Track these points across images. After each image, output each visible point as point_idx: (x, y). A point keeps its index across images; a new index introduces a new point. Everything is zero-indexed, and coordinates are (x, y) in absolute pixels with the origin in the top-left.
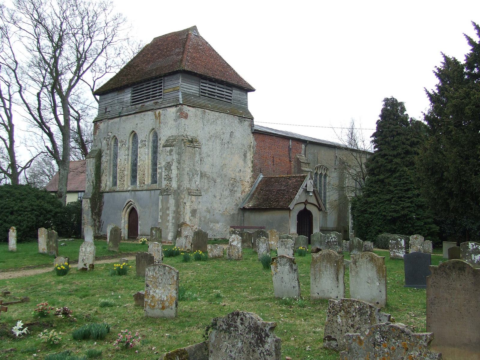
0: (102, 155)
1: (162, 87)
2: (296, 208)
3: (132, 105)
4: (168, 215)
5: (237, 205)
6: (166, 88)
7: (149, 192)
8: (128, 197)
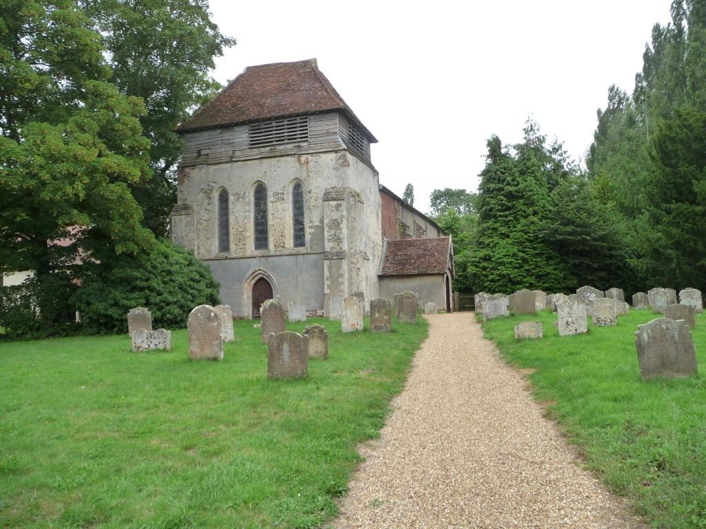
0: (683, 26)
3: (250, 148)
4: (342, 283)
6: (312, 129)
7: (294, 257)
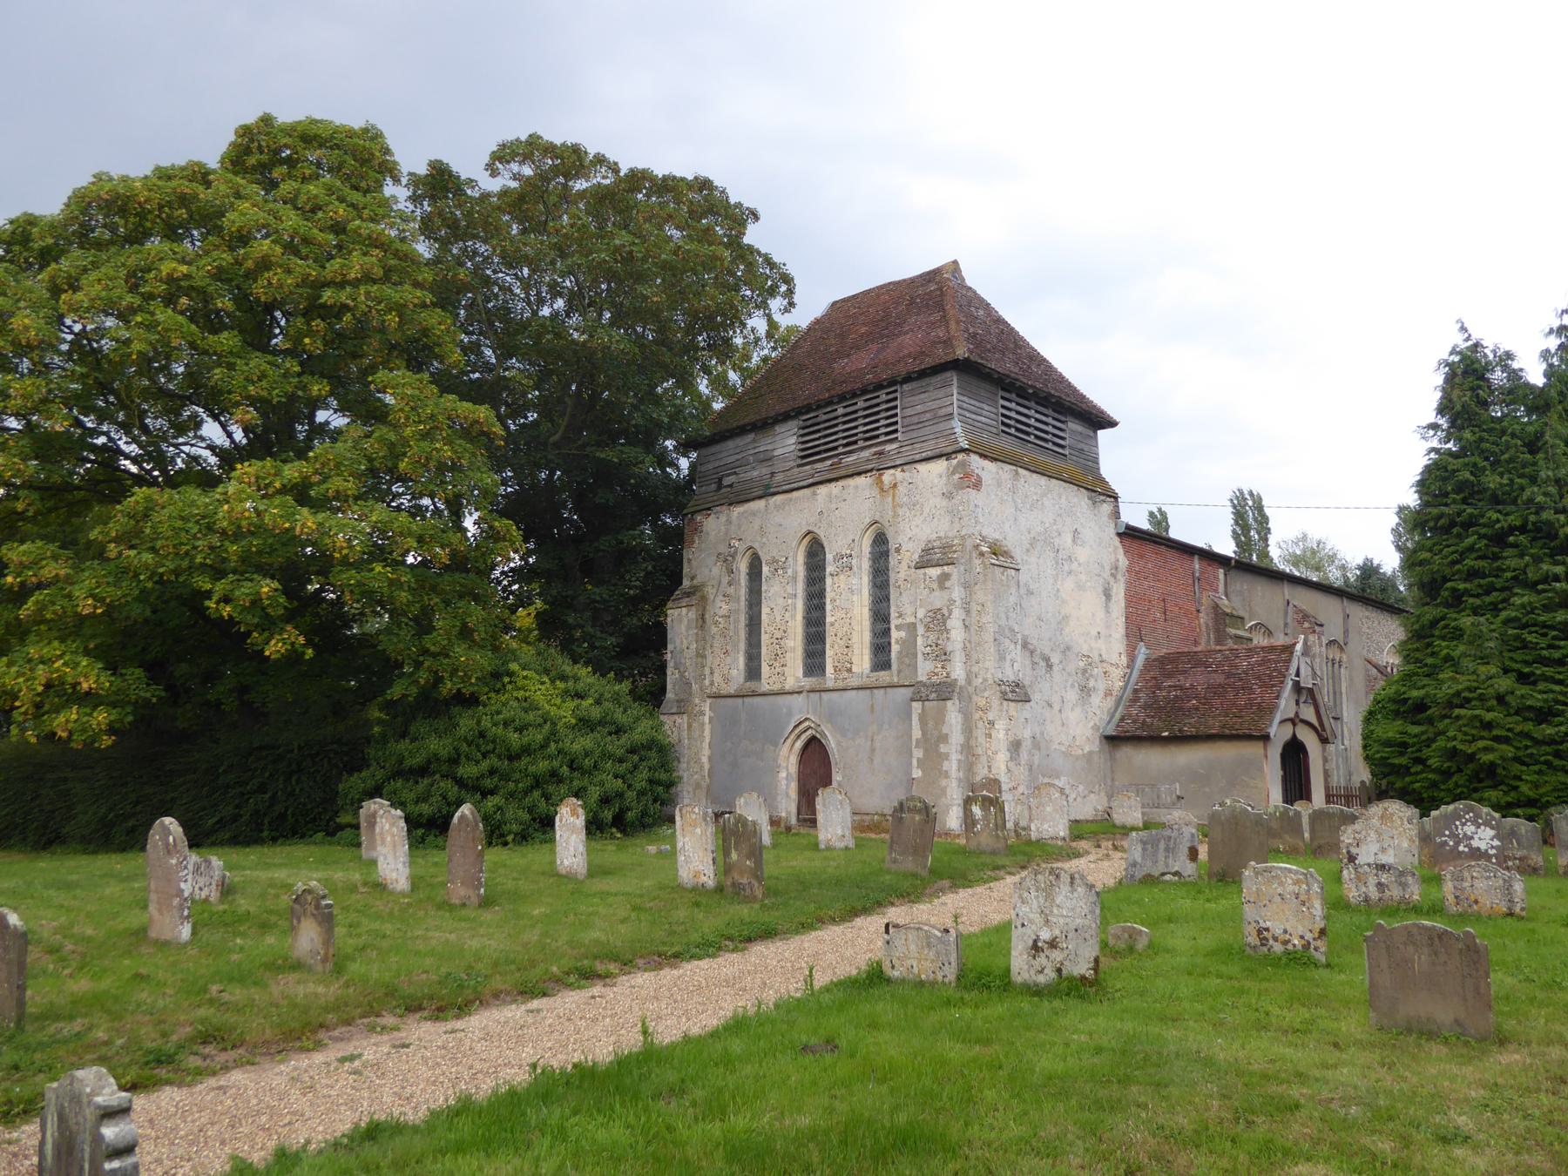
1: (898, 411)
2: (1279, 734)
3: (799, 466)
4: (946, 756)
5: (1095, 728)
7: (868, 691)
8: (799, 707)
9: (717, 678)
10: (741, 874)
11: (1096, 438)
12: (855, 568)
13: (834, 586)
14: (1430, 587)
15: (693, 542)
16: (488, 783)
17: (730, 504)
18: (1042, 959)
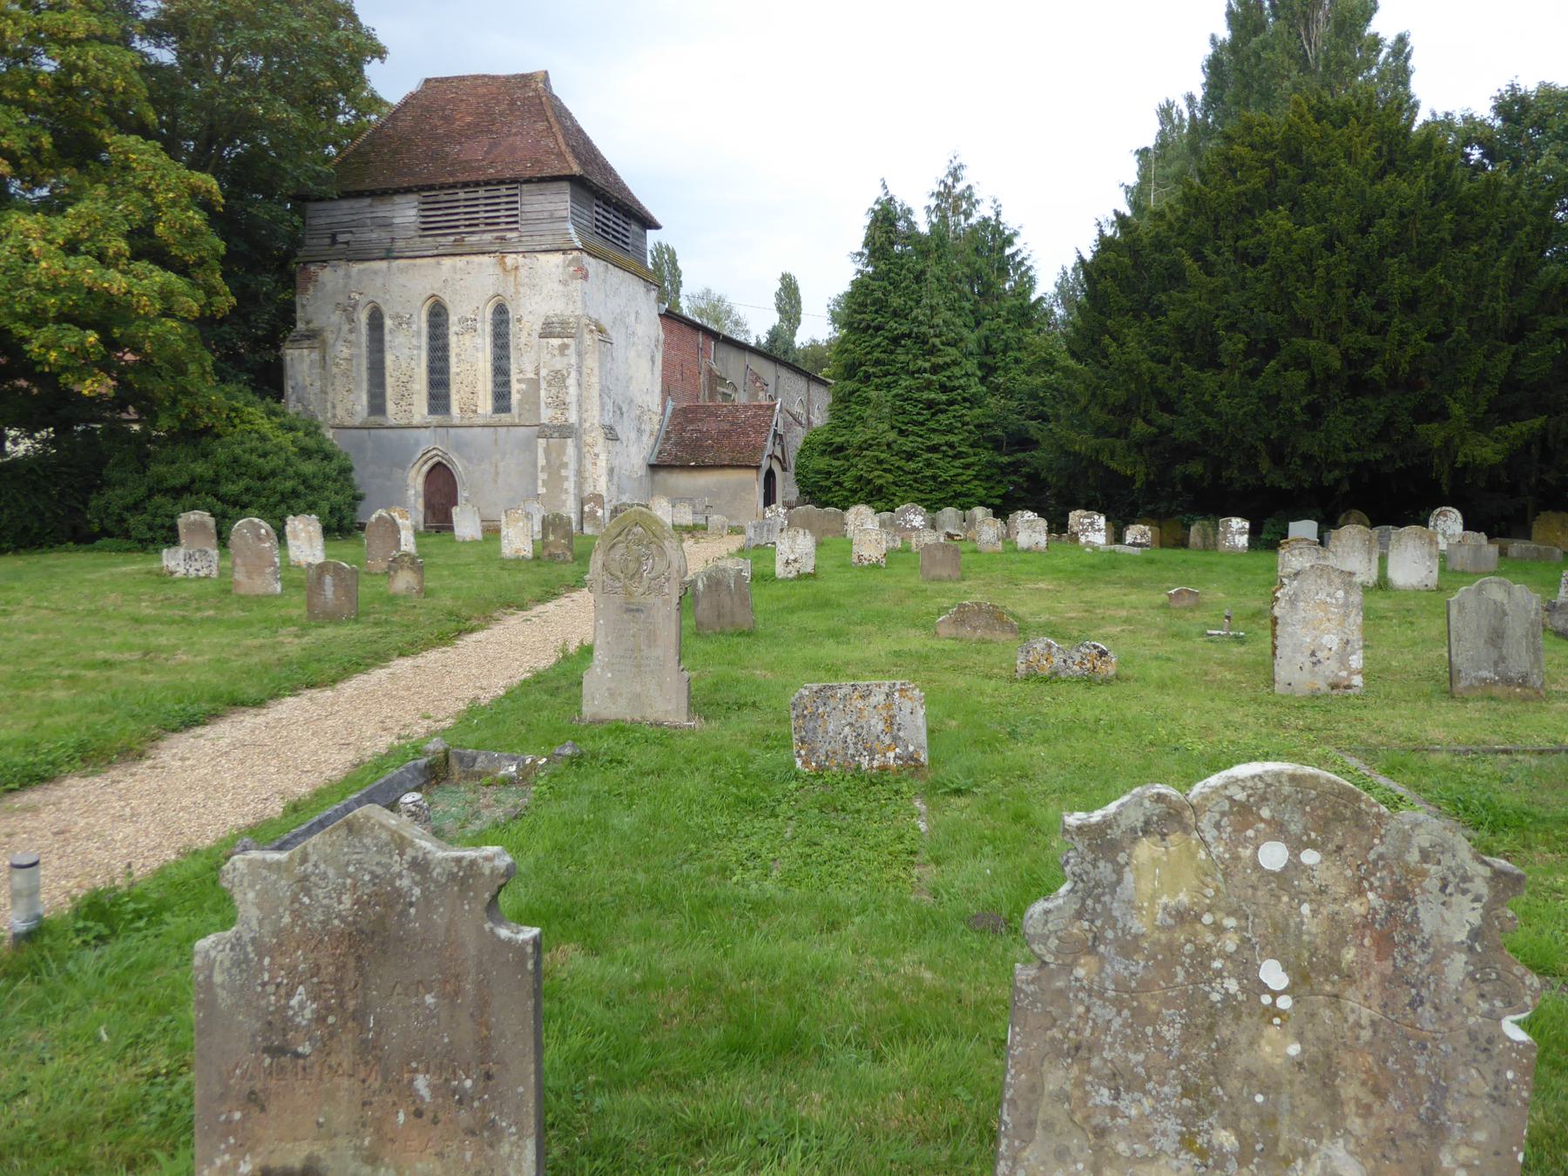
2: (765, 463)
5: (644, 458)
6: (526, 208)
9: (340, 412)
10: (557, 548)
11: (645, 237)
12: (479, 331)
13: (458, 344)
14: (850, 371)
15: (307, 289)
16: (246, 498)
17: (349, 261)
18: (790, 567)
